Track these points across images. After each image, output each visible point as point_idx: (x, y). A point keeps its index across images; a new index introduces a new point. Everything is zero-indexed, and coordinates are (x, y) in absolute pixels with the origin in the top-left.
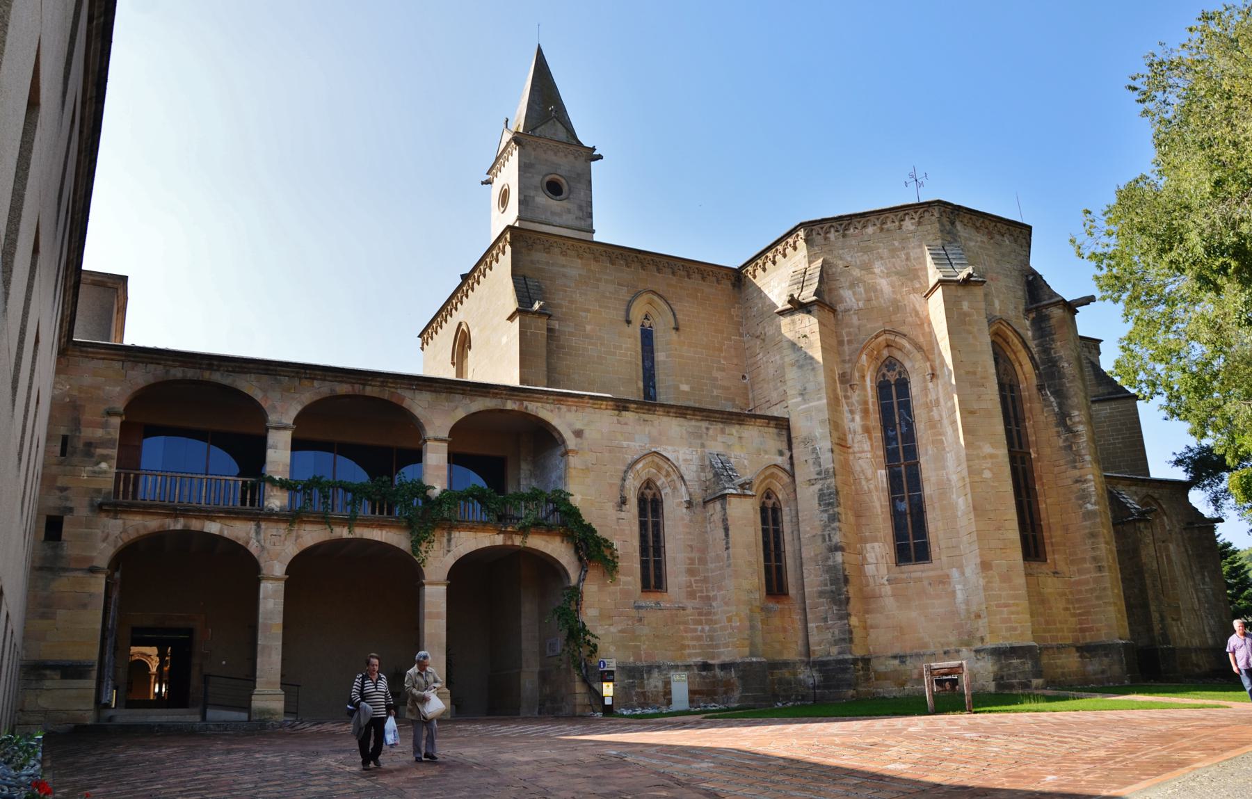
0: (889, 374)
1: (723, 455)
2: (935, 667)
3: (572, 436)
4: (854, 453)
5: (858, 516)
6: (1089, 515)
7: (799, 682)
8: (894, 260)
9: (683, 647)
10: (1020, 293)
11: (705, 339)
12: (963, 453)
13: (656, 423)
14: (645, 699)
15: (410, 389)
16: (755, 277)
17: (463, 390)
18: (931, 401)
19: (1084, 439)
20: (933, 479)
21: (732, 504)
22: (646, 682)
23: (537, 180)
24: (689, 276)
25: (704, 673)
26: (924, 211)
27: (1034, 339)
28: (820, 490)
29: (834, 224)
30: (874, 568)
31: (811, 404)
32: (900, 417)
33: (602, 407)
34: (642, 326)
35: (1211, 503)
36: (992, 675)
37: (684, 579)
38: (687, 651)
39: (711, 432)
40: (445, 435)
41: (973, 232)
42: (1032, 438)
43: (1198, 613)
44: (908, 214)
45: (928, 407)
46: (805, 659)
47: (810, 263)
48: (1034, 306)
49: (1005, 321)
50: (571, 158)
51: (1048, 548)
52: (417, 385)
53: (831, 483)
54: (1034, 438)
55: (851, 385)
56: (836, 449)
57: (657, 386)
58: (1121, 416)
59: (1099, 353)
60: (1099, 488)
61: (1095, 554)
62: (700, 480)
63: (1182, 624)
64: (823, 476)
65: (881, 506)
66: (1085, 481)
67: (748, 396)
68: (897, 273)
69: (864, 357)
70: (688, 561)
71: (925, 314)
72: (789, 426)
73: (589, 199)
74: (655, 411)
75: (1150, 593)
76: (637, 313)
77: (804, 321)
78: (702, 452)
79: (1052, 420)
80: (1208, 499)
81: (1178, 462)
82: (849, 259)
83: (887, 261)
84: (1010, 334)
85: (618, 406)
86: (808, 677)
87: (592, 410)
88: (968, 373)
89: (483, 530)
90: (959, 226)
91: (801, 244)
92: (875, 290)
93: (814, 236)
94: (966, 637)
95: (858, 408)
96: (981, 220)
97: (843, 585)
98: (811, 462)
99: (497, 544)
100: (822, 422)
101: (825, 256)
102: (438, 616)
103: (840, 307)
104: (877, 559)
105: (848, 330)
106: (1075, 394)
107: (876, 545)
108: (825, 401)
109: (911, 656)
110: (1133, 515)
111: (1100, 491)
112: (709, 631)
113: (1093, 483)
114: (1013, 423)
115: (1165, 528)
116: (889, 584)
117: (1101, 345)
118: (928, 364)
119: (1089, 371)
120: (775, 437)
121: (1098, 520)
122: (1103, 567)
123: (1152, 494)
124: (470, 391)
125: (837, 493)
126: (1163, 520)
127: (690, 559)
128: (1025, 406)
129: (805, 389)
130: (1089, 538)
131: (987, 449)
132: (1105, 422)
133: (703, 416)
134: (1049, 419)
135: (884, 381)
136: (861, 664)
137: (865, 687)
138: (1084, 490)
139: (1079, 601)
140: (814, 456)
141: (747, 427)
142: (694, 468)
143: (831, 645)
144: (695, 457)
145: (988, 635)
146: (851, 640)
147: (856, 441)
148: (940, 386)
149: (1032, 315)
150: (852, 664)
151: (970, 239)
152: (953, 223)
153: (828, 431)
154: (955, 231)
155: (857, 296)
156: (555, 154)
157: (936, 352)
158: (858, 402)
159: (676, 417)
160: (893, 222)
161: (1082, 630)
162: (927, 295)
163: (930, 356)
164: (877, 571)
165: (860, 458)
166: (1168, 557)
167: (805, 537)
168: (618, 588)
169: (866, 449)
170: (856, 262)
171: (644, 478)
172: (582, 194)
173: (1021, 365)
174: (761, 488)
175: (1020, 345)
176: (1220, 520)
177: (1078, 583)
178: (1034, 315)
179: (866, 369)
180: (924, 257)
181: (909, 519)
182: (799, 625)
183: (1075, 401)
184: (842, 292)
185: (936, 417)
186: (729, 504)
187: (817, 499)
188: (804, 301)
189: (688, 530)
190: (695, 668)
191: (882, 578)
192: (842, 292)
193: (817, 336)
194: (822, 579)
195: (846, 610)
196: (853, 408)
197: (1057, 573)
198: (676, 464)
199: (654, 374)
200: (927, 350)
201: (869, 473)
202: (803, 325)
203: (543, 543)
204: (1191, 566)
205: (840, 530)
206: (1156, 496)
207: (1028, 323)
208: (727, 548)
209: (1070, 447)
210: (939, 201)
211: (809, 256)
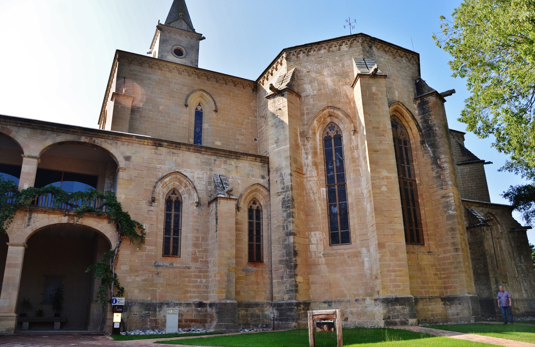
0: (330, 132)
1: (224, 176)
2: (316, 314)
3: (123, 160)
4: (307, 177)
5: (307, 215)
6: (450, 217)
7: (266, 316)
8: (335, 67)
9: (187, 292)
10: (412, 89)
11: (233, 118)
12: (369, 176)
13: (181, 155)
14: (156, 324)
15: (16, 126)
16: (263, 85)
17: (51, 128)
18: (353, 146)
19: (448, 171)
20: (353, 193)
21: (221, 204)
22: (158, 313)
23: (169, 48)
24: (226, 84)
25: (199, 309)
26: (353, 40)
27: (419, 115)
28: (283, 198)
29: (302, 49)
30: (316, 247)
31: (281, 148)
32: (336, 157)
33: (145, 143)
34: (197, 109)
35: (524, 218)
36: (383, 315)
37: (191, 249)
38: (189, 295)
39: (217, 162)
40: (37, 154)
41: (383, 54)
42: (417, 172)
43: (518, 279)
44: (344, 42)
45: (352, 150)
46: (270, 302)
47: (288, 70)
48: (419, 96)
49: (401, 103)
50: (189, 38)
51: (425, 237)
52: (20, 124)
53: (289, 193)
54: (418, 172)
55: (306, 138)
56: (294, 174)
57: (202, 142)
58: (475, 172)
60: (457, 202)
61: (453, 241)
62: (207, 190)
63: (508, 285)
64: (285, 190)
65: (322, 209)
66: (448, 197)
67: (257, 150)
68: (337, 74)
69: (315, 122)
70: (195, 239)
71: (352, 97)
72: (268, 161)
73: (197, 59)
74: (180, 148)
75: (490, 267)
76: (194, 100)
77: (280, 101)
78: (210, 173)
79: (429, 161)
80: (523, 216)
81: (506, 195)
82: (310, 68)
83: (331, 68)
84: (404, 111)
85: (155, 143)
86: (271, 313)
87: (138, 145)
88: (374, 128)
89: (54, 213)
90: (374, 49)
91: (284, 61)
92: (324, 84)
93: (291, 56)
94: (369, 291)
95: (310, 151)
96: (389, 47)
97: (293, 256)
98: (279, 182)
99: (63, 222)
100: (286, 158)
101: (297, 67)
102: (15, 266)
103: (303, 95)
104: (317, 241)
105: (307, 107)
106: (443, 145)
107: (317, 233)
108: (288, 146)
109: (335, 302)
110: (480, 222)
111: (458, 204)
112: (205, 282)
114: (406, 163)
115: (499, 231)
116: (324, 257)
117: (465, 136)
118: (352, 125)
119: (458, 149)
120: (260, 168)
121: (456, 220)
122: (459, 249)
123: (491, 212)
124: (57, 129)
125: (293, 200)
126: (497, 226)
127: (196, 237)
128: (413, 153)
129: (278, 140)
130: (450, 231)
131: (385, 173)
132: (467, 175)
133: (212, 153)
134: (427, 161)
135: (328, 136)
136: (302, 306)
137: (304, 321)
138: (447, 202)
139: (444, 270)
140: (281, 178)
141: (241, 161)
142: (204, 183)
143: (285, 294)
144: (205, 177)
145: (381, 290)
146: (297, 291)
147: (308, 170)
148: (359, 137)
149: (418, 102)
150: (295, 306)
151: (382, 57)
152: (370, 47)
153: (289, 163)
154: (372, 52)
155: (313, 88)
156: (180, 36)
157: (357, 118)
158: (310, 148)
159: (195, 152)
160: (336, 46)
161: (446, 288)
162: (353, 85)
163: (354, 121)
164: (317, 248)
165: (310, 181)
167: (273, 227)
168: (144, 253)
169: (314, 175)
170: (313, 69)
171: (171, 188)
172: (193, 56)
173: (411, 130)
174: (249, 197)
176: (530, 228)
177: (444, 258)
178: (419, 102)
179: (317, 129)
180: (352, 65)
181: (339, 218)
182: (268, 281)
183: (442, 149)
184: (305, 86)
185: (356, 156)
186: (219, 204)
188: (281, 89)
189: (196, 220)
190: (193, 305)
191: (320, 253)
192: (305, 86)
193: (287, 108)
194: (281, 252)
195: (294, 272)
196: (308, 151)
197: (430, 252)
198: (192, 180)
199: (201, 136)
200: (352, 117)
201: (315, 189)
202: (279, 103)
203: (95, 223)
205: (293, 222)
206: (494, 213)
207: (416, 106)
208: (216, 231)
209: (439, 177)
210: (361, 34)
211: (288, 68)
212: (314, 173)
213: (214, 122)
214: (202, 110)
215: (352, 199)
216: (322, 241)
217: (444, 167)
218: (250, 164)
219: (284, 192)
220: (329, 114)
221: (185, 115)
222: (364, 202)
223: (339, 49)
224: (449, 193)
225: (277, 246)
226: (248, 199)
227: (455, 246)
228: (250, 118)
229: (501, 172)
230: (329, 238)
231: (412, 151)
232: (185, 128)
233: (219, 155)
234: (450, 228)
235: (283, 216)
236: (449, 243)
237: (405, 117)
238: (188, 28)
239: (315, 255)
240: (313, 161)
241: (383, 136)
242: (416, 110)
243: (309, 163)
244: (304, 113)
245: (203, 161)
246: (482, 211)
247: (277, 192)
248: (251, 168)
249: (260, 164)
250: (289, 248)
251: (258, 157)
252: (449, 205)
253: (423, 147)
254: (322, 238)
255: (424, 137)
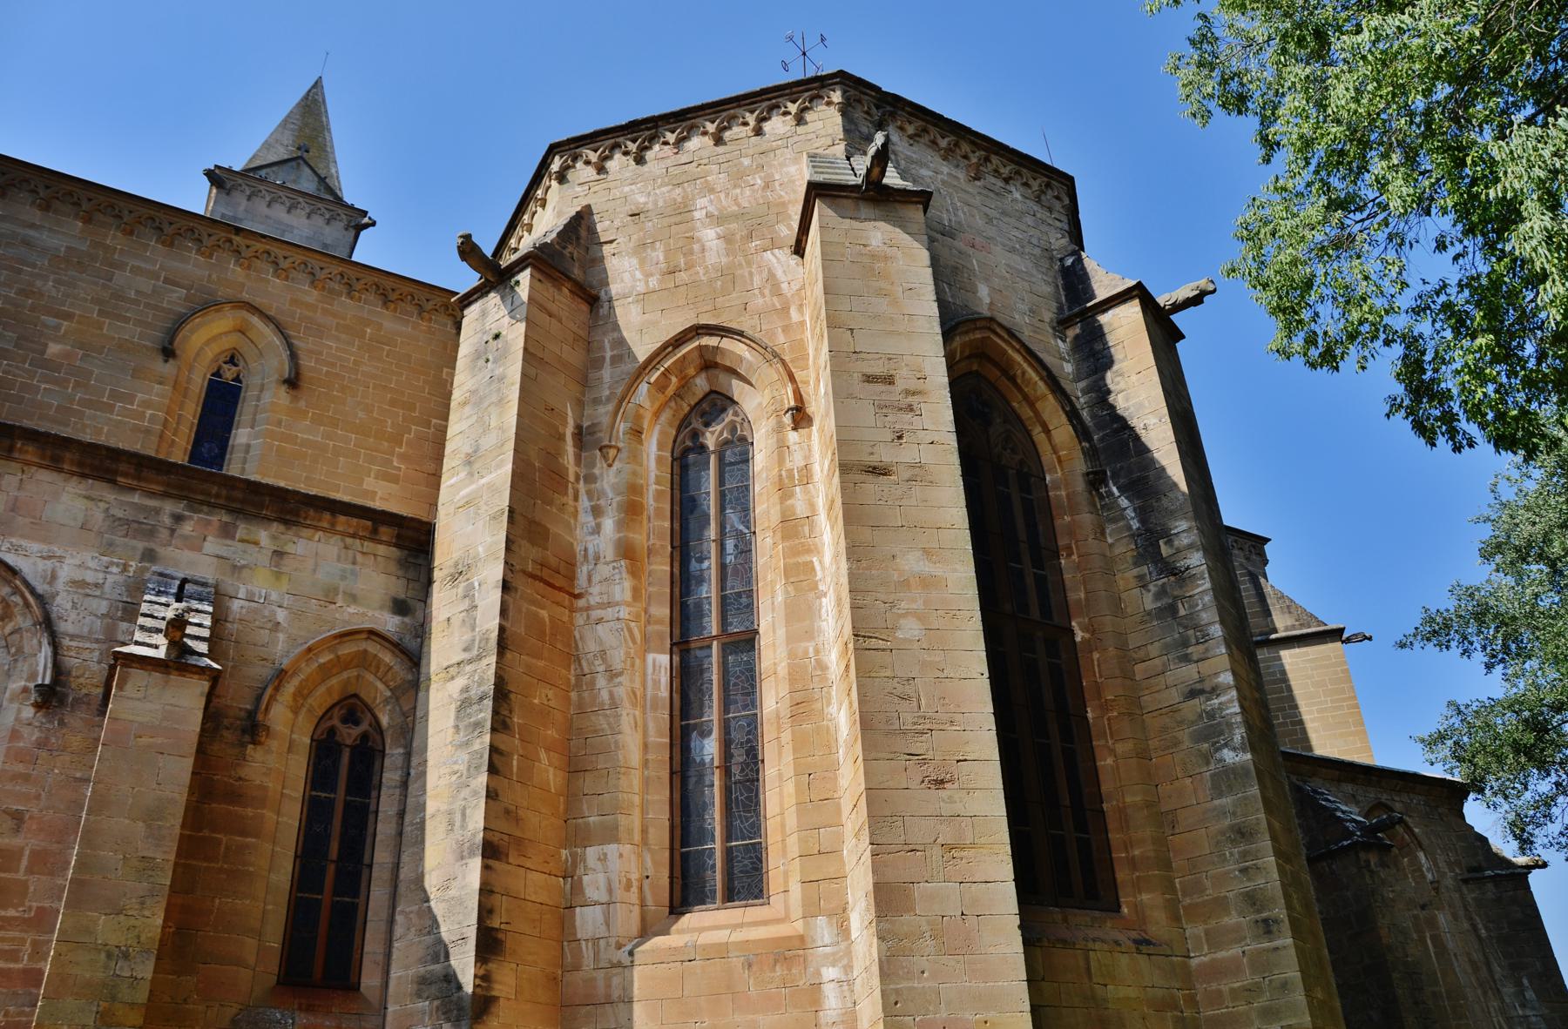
4: (588, 608)
6: (1227, 779)
10: (1048, 289)
19: (1206, 584)
28: (466, 689)
30: (600, 919)
34: (217, 374)
39: (187, 528)
42: (1077, 595)
45: (784, 489)
59: (1266, 562)
61: (1250, 885)
64: (475, 652)
66: (1215, 691)
69: (643, 388)
83: (722, 196)
88: (870, 379)
104: (610, 891)
107: (611, 849)
113: (1234, 693)
115: (1424, 877)
117: (1268, 548)
120: (393, 567)
122: (1276, 921)
123: (1389, 803)
128: (1058, 523)
138: (1211, 715)
141: (306, 532)
142: (103, 607)
147: (596, 578)
149: (1072, 332)
164: (608, 925)
165: (599, 621)
166: (1436, 939)
169: (618, 597)
173: (1047, 431)
175: (1041, 384)
185: (800, 508)
187: (452, 714)
196: (602, 502)
201: (618, 658)
204: (1488, 964)
209: (1172, 610)
212: (622, 589)
213: (279, 423)
214: (240, 382)
215: (777, 693)
216: (634, 889)
217: (1188, 568)
218: (346, 548)
219: (470, 662)
220: (701, 356)
221: (157, 386)
222: (829, 704)
223: (758, 132)
224: (1217, 674)
225: (415, 908)
226: (321, 699)
227: (1259, 911)
228: (434, 421)
229: (1407, 650)
230: (671, 877)
231: (1054, 513)
232: (148, 431)
233: (200, 497)
234: (1232, 827)
235: (456, 767)
236: (1230, 895)
237: (1019, 381)
238: (319, 190)
239: (596, 954)
240: (620, 539)
241: (912, 410)
242: (1069, 361)
243: (602, 546)
244: (604, 358)
245: (120, 514)
246: (1354, 796)
247: (445, 665)
248: (350, 567)
249: (394, 552)
250: (461, 917)
251: (384, 523)
252: (1219, 723)
253: (1097, 499)
254: (634, 876)
255: (1102, 457)
